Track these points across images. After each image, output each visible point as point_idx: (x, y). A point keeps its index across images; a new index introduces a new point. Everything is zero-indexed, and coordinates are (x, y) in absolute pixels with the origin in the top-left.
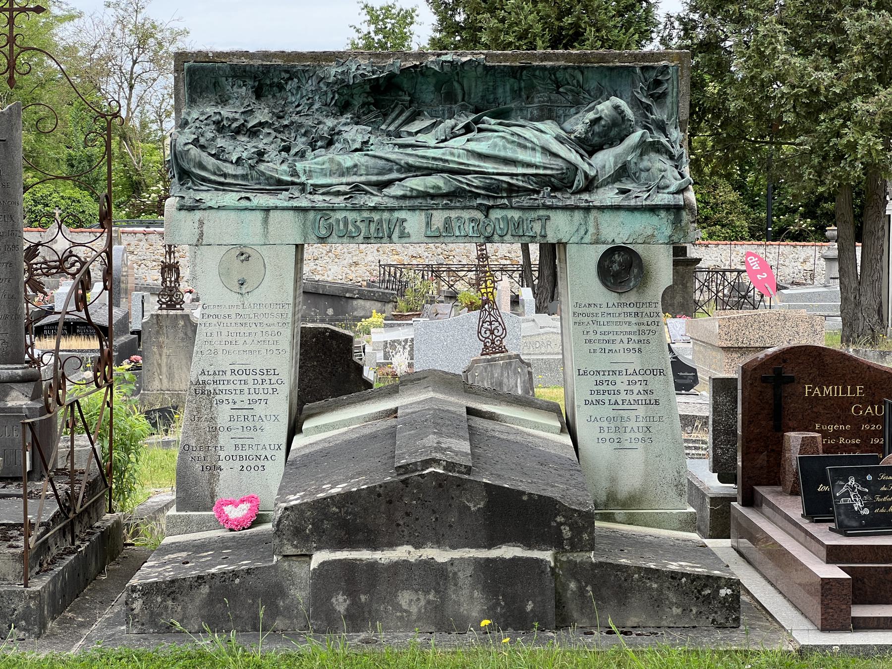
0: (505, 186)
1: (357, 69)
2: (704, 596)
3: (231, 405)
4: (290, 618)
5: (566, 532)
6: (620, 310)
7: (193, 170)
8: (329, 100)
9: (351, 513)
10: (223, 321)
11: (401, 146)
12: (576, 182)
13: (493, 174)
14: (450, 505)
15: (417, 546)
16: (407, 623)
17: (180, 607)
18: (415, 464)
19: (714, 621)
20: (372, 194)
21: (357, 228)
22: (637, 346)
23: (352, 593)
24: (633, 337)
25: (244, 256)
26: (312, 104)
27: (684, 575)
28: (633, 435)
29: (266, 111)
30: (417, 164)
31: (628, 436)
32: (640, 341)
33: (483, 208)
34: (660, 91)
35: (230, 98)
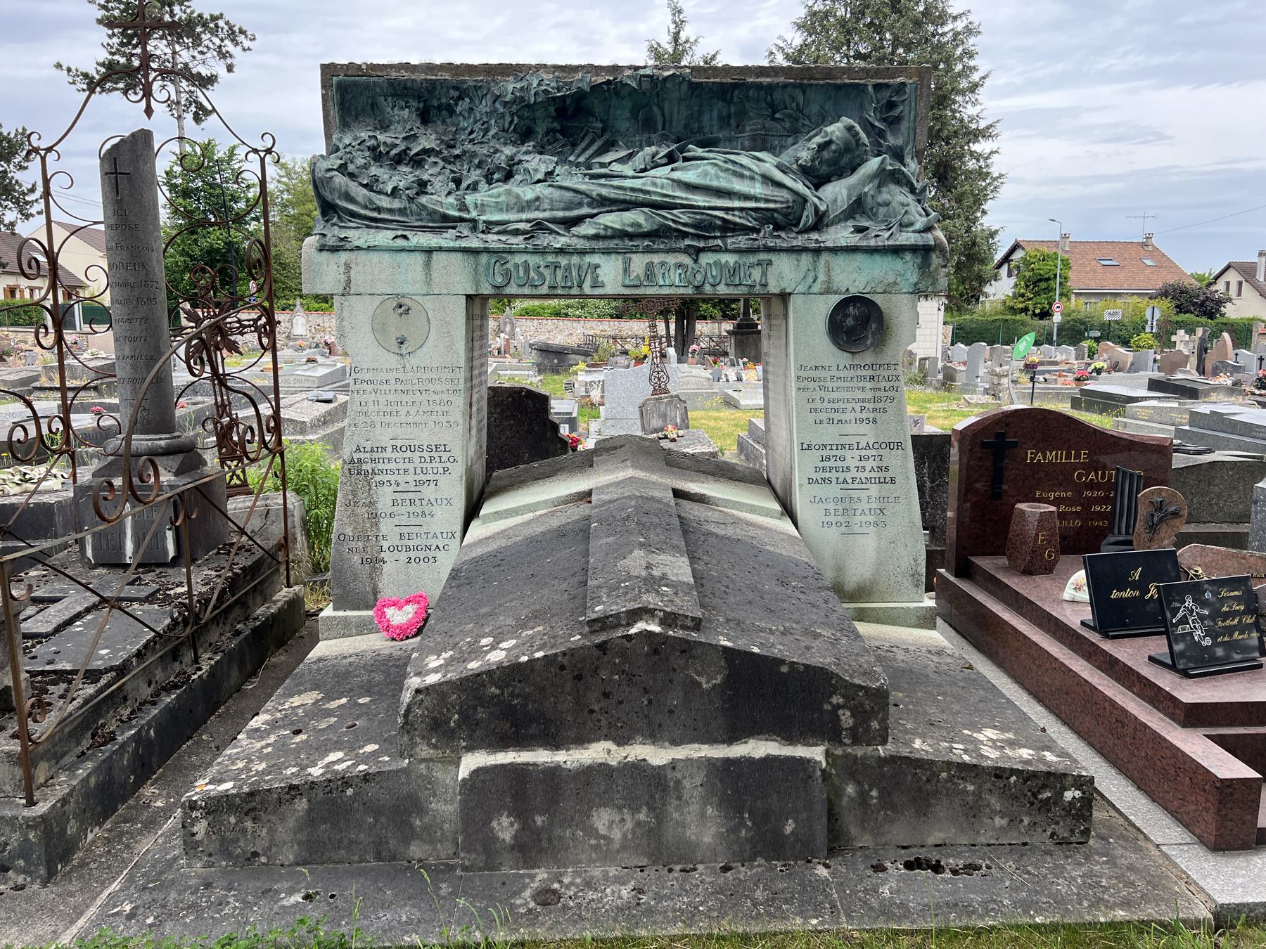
0: (719, 222)
1: (539, 85)
2: (1041, 801)
3: (394, 488)
4: (431, 842)
5: (846, 718)
6: (852, 373)
7: (338, 202)
8: (507, 125)
9: (518, 695)
10: (380, 387)
11: (593, 177)
12: (804, 218)
13: (705, 208)
14: (671, 681)
15: (621, 741)
16: (605, 852)
17: (265, 831)
18: (617, 615)
19: (1052, 836)
20: (558, 233)
21: (541, 275)
22: (871, 416)
23: (521, 813)
24: (867, 405)
25: (403, 309)
26: (487, 131)
27: (1013, 772)
28: (864, 519)
29: (433, 137)
30: (612, 196)
31: (858, 519)
32: (875, 410)
33: (692, 251)
34: (896, 113)
35: (391, 123)
